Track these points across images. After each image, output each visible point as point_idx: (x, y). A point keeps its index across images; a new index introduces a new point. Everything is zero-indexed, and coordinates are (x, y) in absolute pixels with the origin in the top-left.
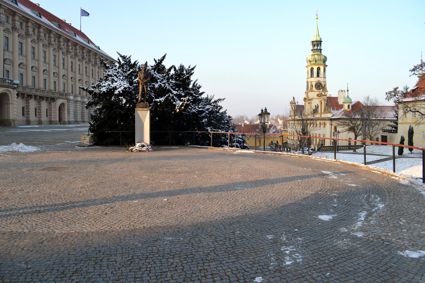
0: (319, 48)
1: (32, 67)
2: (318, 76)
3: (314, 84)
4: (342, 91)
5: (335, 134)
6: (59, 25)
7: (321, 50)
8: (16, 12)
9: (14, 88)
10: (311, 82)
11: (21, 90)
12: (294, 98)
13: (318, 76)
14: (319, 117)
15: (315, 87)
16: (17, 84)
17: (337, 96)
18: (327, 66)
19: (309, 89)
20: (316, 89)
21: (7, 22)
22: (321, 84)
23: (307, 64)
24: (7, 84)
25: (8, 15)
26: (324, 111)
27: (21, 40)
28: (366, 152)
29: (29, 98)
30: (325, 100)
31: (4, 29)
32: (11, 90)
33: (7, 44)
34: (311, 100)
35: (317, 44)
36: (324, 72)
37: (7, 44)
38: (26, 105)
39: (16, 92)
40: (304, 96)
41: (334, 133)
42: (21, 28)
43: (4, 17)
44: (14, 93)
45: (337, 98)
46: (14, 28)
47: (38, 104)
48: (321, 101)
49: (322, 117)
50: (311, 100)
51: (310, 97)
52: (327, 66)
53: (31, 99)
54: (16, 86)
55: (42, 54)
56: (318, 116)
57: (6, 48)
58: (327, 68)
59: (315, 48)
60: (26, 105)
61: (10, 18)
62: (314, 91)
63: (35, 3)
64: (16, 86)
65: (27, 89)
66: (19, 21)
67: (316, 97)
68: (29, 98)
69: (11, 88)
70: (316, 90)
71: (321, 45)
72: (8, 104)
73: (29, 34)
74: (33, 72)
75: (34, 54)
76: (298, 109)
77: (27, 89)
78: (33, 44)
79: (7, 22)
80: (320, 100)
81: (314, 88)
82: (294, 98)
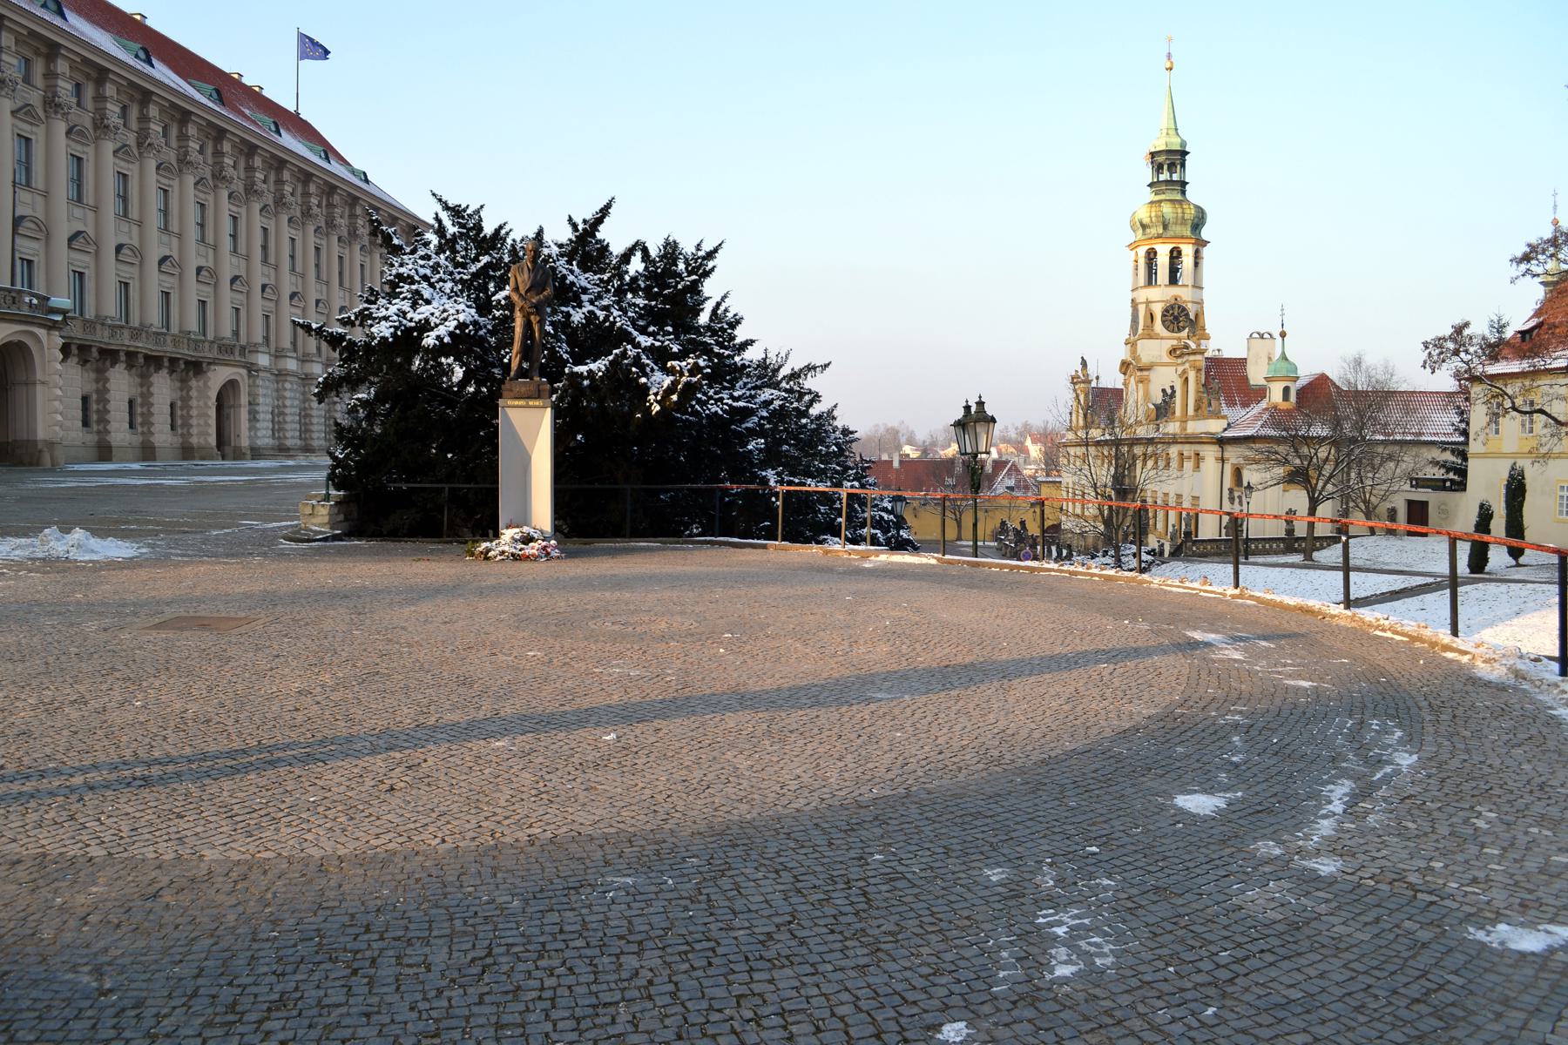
0: (1175, 177)
1: (119, 248)
2: (1173, 280)
3: (1158, 310)
4: (1262, 336)
5: (1236, 494)
6: (218, 91)
7: (1183, 184)
8: (59, 46)
9: (52, 326)
10: (1148, 303)
11: (76, 331)
12: (1084, 363)
13: (1173, 280)
14: (1178, 431)
15: (1163, 322)
16: (63, 312)
17: (1244, 356)
18: (1205, 243)
19: (1140, 327)
20: (1167, 328)
21: (27, 80)
22: (1184, 309)
23: (1131, 237)
24: (26, 311)
25: (29, 54)
26: (1196, 410)
27: (79, 147)
28: (1352, 563)
29: (108, 363)
30: (1199, 370)
31: (15, 107)
32: (41, 332)
33: (26, 164)
34: (1148, 368)
35: (1169, 162)
36: (1196, 264)
37: (26, 164)
38: (94, 386)
39: (60, 341)
40: (1123, 353)
41: (1231, 491)
42: (79, 104)
43: (15, 62)
44: (51, 342)
45: (1242, 362)
46: (52, 104)
47: (142, 385)
48: (1184, 372)
49: (1189, 431)
50: (1148, 368)
51: (1145, 359)
52: (1205, 243)
53: (113, 364)
54: (59, 318)
55: (154, 201)
56: (1172, 428)
57: (24, 177)
58: (1205, 251)
59: (1162, 177)
60: (94, 386)
61: (39, 68)
62: (1157, 337)
63: (128, 9)
64: (59, 318)
65: (98, 327)
66: (71, 78)
67: (1166, 359)
68: (108, 363)
69: (41, 326)
70: (1165, 333)
71: (1183, 165)
72: (30, 384)
73: (107, 127)
74: (123, 267)
75: (124, 198)
76: (1100, 403)
77: (98, 327)
78: (122, 164)
79: (27, 80)
80: (1180, 369)
81: (1158, 327)
82: (1084, 363)
